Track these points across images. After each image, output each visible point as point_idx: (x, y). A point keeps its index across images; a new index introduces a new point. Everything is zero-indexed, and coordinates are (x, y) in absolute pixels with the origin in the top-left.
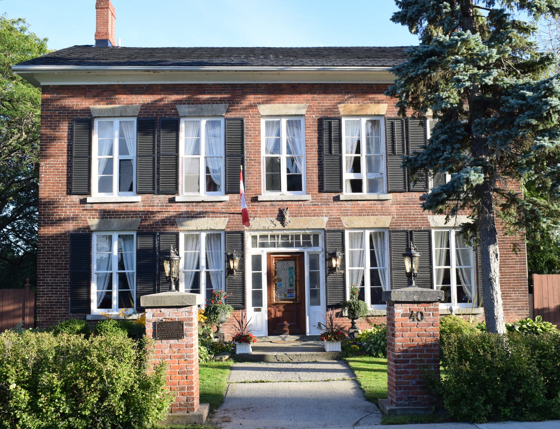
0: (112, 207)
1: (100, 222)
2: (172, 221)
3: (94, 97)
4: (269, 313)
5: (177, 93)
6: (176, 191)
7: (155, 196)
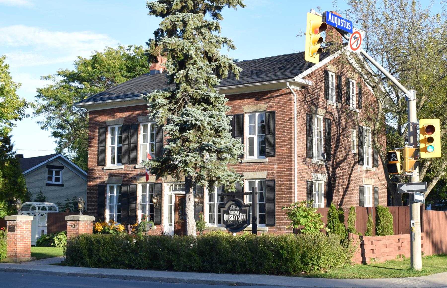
0: (113, 171)
1: (108, 179)
2: (136, 178)
3: (107, 115)
4: (175, 227)
5: (138, 110)
6: (136, 163)
7: (129, 165)
